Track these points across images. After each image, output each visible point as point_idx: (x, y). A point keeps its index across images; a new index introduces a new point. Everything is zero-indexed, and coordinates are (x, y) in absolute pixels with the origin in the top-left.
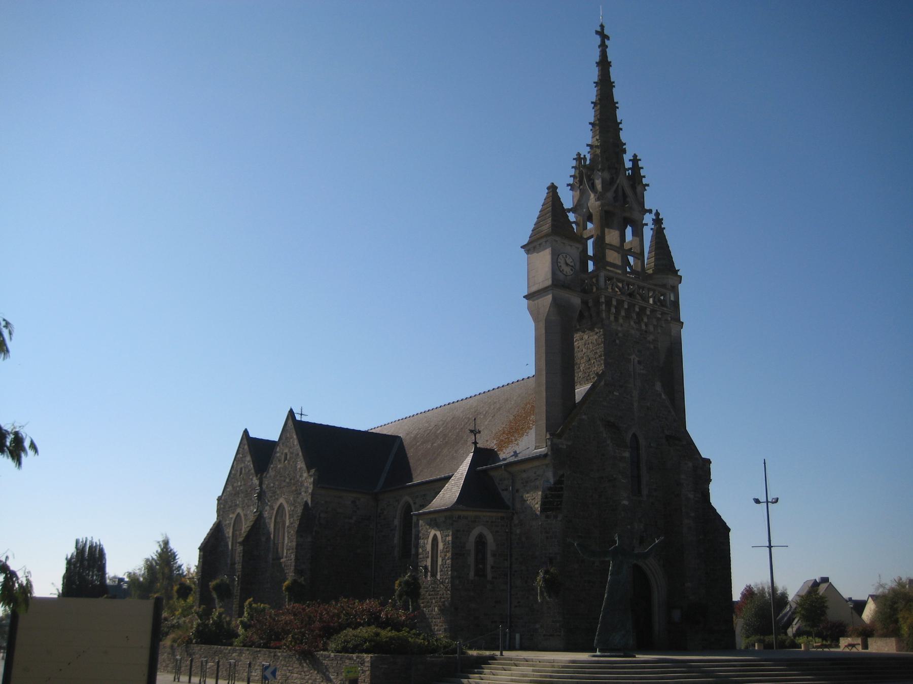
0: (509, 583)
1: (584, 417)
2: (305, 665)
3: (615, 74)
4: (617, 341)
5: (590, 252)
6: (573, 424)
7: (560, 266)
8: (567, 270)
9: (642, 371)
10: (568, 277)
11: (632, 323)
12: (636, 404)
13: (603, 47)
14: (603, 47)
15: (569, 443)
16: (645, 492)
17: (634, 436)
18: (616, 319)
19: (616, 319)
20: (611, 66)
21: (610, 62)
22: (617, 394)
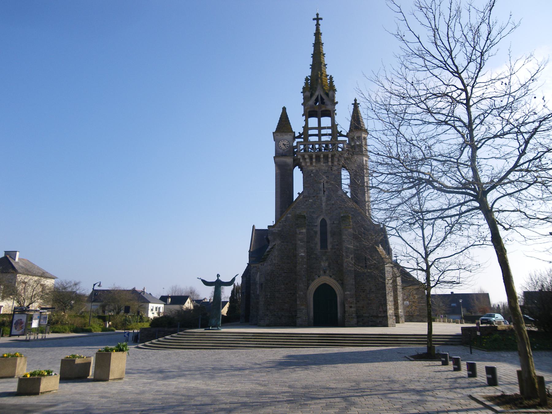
0: (332, 400)
1: (289, 215)
2: (85, 304)
3: (323, 39)
4: (312, 175)
5: (415, 183)
6: (282, 219)
7: (280, 146)
8: (283, 147)
9: (330, 186)
10: (285, 150)
11: (322, 164)
12: (324, 204)
13: (318, 25)
14: (318, 25)
15: (279, 229)
16: (329, 247)
17: (323, 221)
18: (311, 163)
19: (311, 163)
20: (314, 33)
21: (321, 33)
22: (312, 201)
